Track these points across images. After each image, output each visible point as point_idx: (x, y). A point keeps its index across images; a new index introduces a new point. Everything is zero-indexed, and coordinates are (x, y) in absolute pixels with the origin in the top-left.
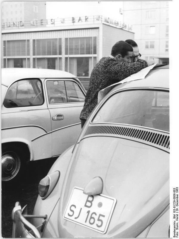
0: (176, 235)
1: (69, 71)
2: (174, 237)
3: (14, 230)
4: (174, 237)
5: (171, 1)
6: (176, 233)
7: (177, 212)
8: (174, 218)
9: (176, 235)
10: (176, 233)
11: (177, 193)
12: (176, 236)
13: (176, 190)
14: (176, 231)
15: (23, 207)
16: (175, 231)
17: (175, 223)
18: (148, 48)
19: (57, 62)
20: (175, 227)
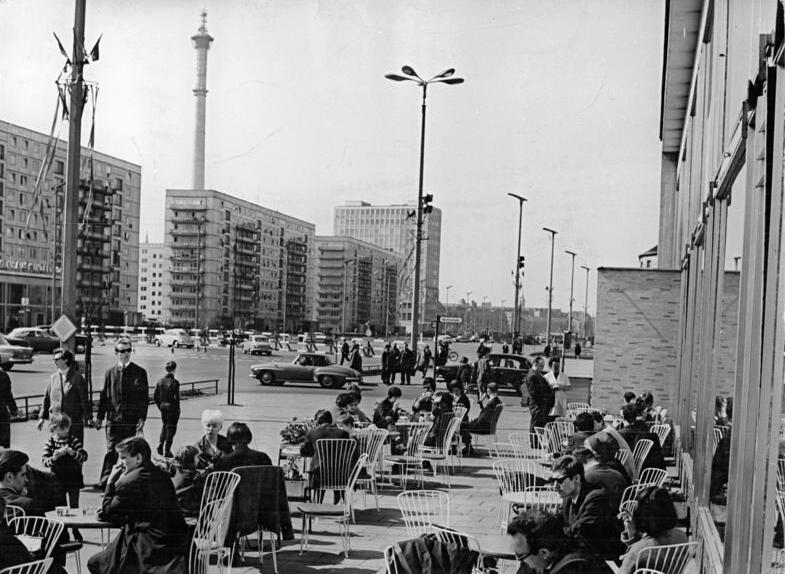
18: (378, 211)
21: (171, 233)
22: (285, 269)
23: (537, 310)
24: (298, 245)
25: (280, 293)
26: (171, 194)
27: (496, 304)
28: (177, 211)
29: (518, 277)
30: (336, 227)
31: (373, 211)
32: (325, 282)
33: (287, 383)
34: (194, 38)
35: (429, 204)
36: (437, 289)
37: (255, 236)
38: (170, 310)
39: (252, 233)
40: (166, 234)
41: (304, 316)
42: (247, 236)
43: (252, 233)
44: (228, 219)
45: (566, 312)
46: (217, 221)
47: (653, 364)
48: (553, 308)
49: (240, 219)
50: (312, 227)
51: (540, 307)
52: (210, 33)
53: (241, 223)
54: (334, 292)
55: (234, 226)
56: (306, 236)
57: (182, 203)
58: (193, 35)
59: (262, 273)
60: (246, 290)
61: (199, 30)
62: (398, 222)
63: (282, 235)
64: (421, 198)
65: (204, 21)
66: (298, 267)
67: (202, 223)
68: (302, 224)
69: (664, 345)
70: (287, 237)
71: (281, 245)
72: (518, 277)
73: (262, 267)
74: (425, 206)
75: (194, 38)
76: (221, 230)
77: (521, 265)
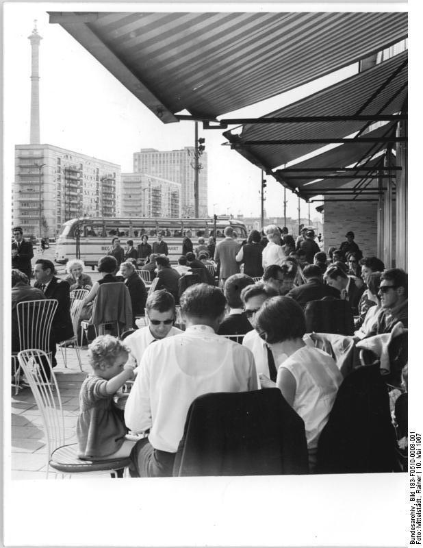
0: (416, 538)
1: (397, 49)
2: (412, 543)
3: (93, 423)
4: (412, 543)
5: (405, 4)
6: (416, 535)
7: (419, 470)
8: (412, 500)
9: (416, 538)
10: (416, 535)
11: (418, 448)
12: (415, 541)
13: (416, 440)
14: (417, 530)
15: (393, 61)
16: (413, 529)
17: (413, 511)
18: (164, 155)
19: (186, 70)
20: (413, 521)
21: (19, 175)
22: (100, 196)
23: (275, 218)
24: (109, 180)
25: (98, 213)
26: (19, 148)
27: (247, 215)
28: (21, 158)
29: (262, 194)
30: (135, 166)
31: (160, 155)
32: (129, 210)
33: (112, 222)
34: (29, 38)
35: (203, 144)
36: (206, 206)
37: (78, 190)
38: (19, 218)
39: (76, 172)
40: (16, 175)
41: (115, 215)
42: (73, 183)
43: (76, 172)
44: (59, 163)
45: (295, 219)
46: (51, 191)
47: (363, 234)
48: (287, 216)
49: (66, 163)
50: (118, 167)
51: (276, 217)
52: (40, 34)
53: (68, 166)
54: (135, 210)
55: (64, 168)
56: (114, 173)
57: (26, 154)
58: (29, 36)
59: (84, 199)
60: (74, 212)
61: (12, 249)
62: (178, 162)
63: (98, 173)
64: (196, 141)
65: (36, 26)
66: (109, 202)
67: (41, 167)
68: (112, 165)
69: (369, 220)
70: (101, 175)
71: (97, 180)
72: (262, 194)
73: (84, 196)
74: (199, 145)
75: (29, 38)
76: (54, 171)
77: (265, 186)
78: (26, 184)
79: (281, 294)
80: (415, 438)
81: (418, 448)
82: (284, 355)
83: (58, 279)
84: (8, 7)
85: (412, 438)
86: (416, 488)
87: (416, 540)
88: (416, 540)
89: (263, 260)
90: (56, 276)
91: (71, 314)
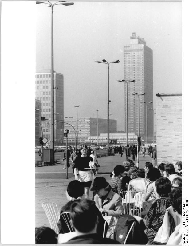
0: (186, 242)
6: (186, 240)
9: (186, 242)
10: (186, 240)
11: (187, 207)
48: (110, 119)
61: (37, 145)
78: (41, 82)
79: (124, 232)
80: (186, 203)
81: (187, 207)
82: (61, 229)
83: (82, 178)
84: (3, 3)
85: (184, 203)
86: (186, 225)
87: (186, 242)
88: (186, 242)
89: (117, 125)
90: (82, 178)
91: (132, 216)
